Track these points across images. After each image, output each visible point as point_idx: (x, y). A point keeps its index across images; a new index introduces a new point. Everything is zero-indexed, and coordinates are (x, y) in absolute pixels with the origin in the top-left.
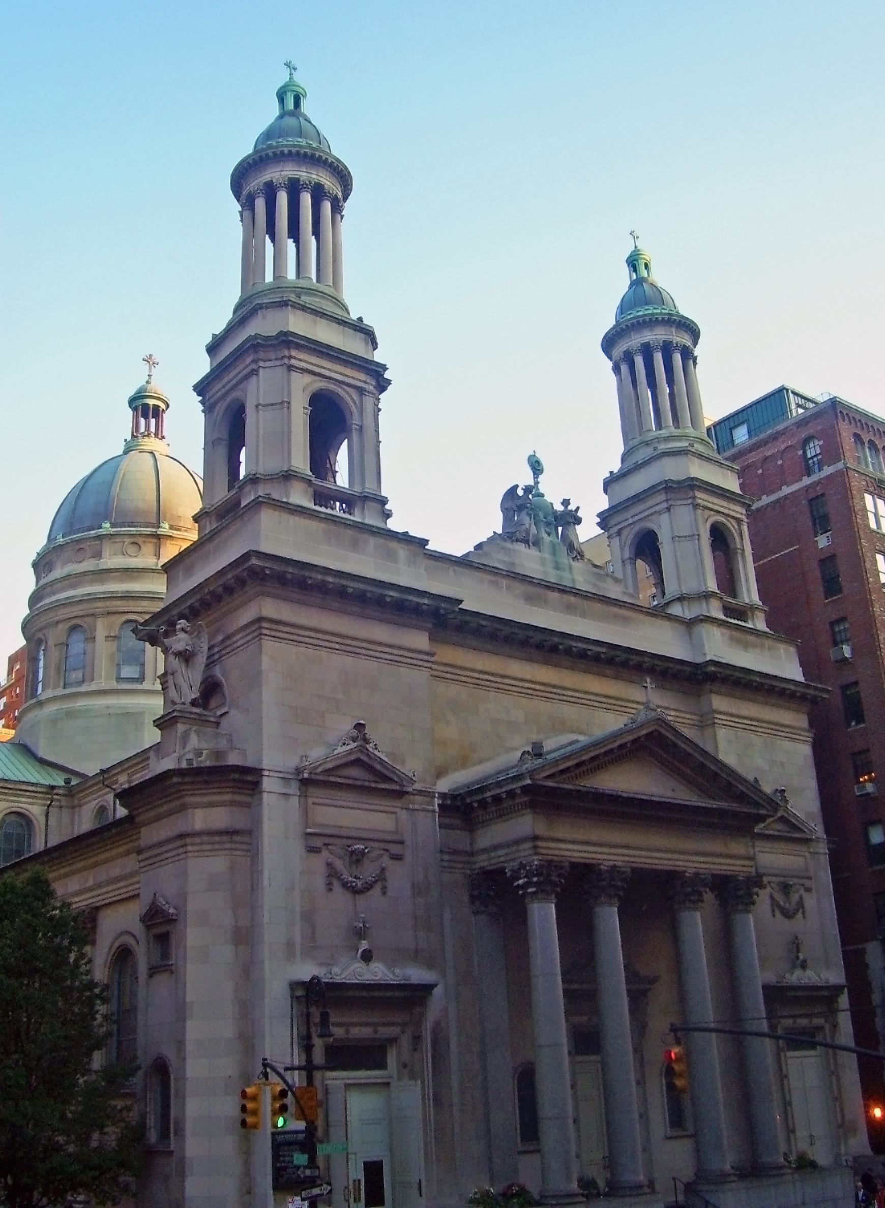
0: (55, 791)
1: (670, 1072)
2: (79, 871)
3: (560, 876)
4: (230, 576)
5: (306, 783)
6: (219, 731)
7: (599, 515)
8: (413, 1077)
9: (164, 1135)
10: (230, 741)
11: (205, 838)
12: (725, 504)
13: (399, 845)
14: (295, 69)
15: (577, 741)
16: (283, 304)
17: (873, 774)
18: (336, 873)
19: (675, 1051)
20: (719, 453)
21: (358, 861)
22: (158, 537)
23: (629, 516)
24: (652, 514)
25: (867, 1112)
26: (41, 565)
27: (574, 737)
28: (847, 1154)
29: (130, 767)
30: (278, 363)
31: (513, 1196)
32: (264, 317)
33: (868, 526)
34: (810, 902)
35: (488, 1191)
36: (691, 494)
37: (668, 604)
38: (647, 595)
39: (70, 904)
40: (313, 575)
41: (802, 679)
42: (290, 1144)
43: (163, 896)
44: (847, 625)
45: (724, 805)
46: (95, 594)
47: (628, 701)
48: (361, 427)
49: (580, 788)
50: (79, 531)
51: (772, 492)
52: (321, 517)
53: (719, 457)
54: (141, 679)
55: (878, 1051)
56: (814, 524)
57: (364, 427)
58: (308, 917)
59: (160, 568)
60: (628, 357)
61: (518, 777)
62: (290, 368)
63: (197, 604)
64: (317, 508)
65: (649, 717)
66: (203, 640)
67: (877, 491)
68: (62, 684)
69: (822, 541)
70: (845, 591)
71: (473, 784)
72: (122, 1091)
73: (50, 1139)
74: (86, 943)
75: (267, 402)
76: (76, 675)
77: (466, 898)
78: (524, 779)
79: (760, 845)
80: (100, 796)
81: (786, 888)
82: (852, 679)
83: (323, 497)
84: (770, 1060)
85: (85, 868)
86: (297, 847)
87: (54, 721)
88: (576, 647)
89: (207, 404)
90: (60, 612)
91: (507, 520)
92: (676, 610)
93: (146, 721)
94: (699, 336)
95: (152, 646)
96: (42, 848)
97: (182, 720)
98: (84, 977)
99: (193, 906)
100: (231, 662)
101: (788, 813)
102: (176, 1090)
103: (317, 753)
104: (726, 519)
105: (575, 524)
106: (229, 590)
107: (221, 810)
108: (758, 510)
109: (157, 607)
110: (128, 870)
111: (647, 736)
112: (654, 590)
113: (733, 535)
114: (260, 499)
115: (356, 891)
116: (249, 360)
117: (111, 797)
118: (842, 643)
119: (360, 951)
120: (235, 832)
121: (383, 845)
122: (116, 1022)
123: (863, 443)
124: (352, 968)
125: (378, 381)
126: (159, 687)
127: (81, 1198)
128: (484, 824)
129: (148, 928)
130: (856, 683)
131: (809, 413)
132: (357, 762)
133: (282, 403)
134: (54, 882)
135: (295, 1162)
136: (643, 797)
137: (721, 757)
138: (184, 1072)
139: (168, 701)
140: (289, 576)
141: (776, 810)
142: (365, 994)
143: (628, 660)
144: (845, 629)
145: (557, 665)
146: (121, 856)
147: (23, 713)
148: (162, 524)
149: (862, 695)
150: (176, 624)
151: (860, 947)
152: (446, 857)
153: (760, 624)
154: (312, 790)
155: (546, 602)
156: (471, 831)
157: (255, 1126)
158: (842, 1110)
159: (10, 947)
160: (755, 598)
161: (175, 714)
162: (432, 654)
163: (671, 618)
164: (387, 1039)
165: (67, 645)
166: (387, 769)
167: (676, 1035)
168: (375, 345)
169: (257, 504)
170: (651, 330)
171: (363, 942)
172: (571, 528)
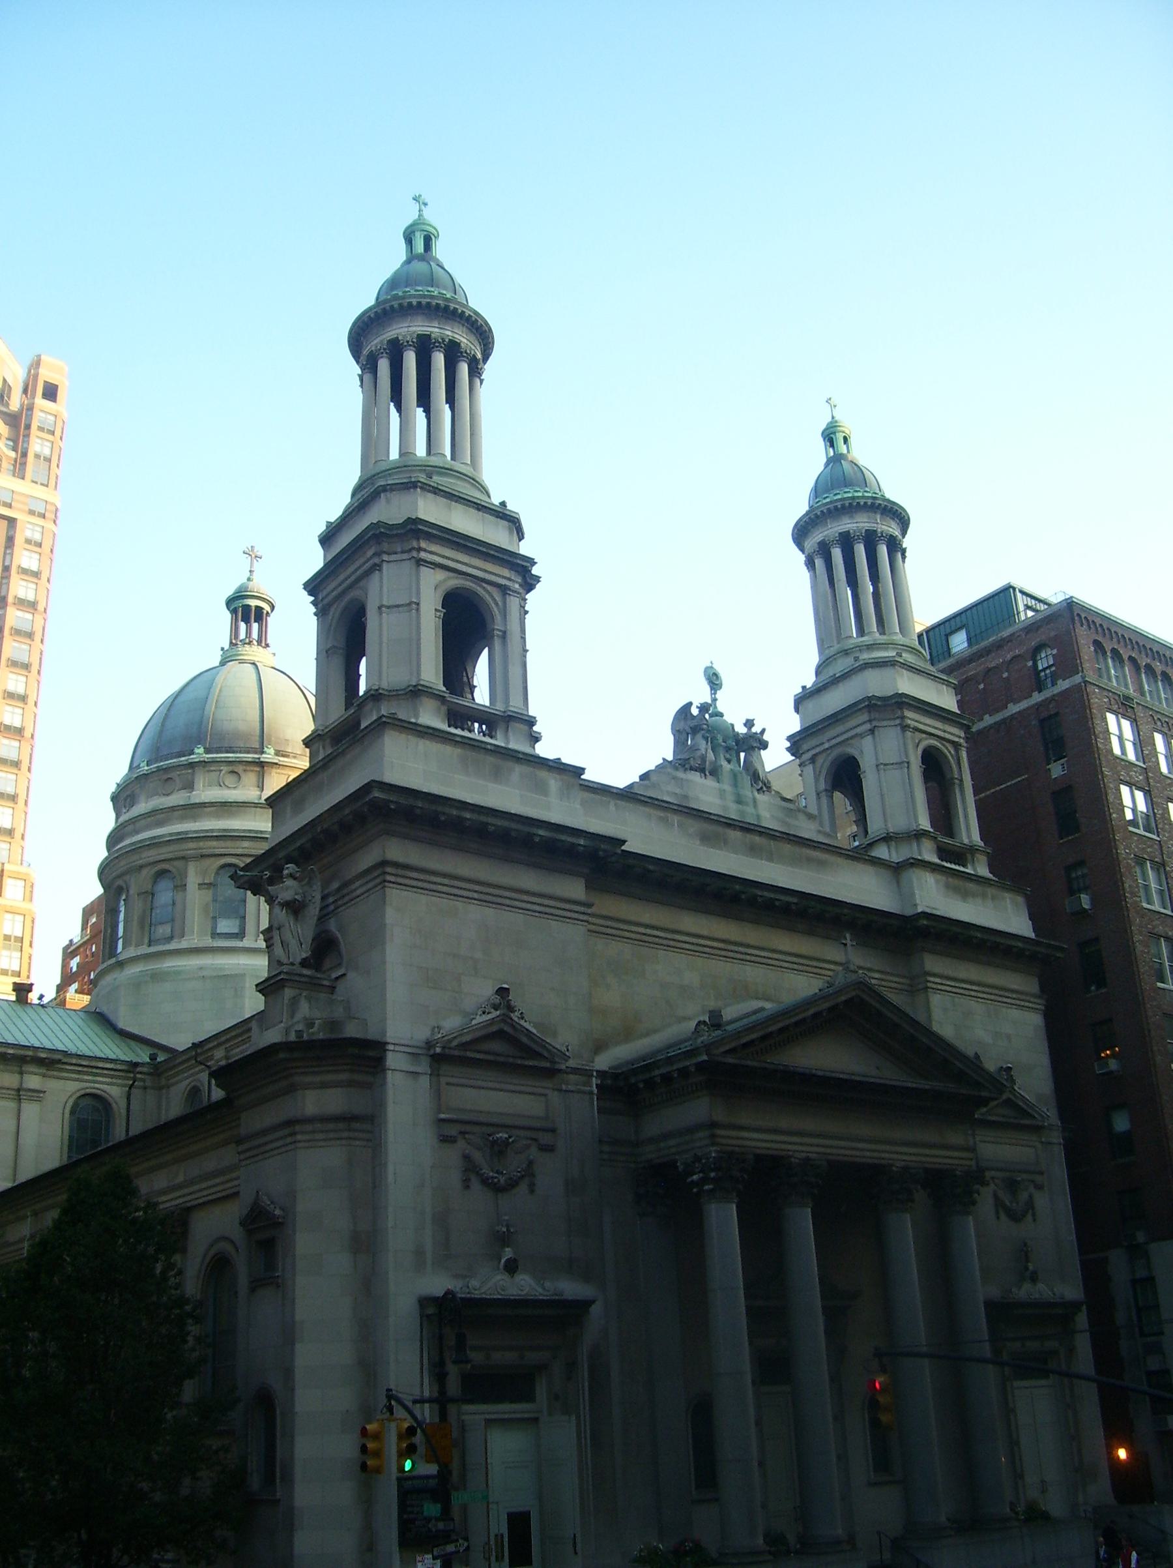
0: (139, 1069)
1: (873, 1405)
4: (347, 811)
7: (789, 738)
9: (269, 1478)
11: (318, 1126)
14: (425, 204)
15: (762, 1009)
16: (412, 486)
20: (932, 665)
22: (262, 765)
23: (825, 740)
24: (852, 738)
26: (122, 798)
29: (228, 1040)
30: (405, 556)
32: (388, 501)
34: (1041, 1201)
35: (656, 1548)
36: (899, 713)
37: (871, 845)
38: (846, 834)
39: (157, 1204)
40: (447, 810)
41: (1032, 935)
44: (1085, 871)
46: (187, 833)
48: (505, 632)
49: (767, 1066)
51: (997, 711)
53: (932, 669)
54: (241, 935)
57: (508, 633)
58: (442, 1220)
59: (264, 802)
60: (824, 550)
62: (419, 562)
64: (453, 730)
66: (315, 887)
68: (146, 941)
69: (1057, 770)
75: (391, 603)
76: (163, 930)
80: (192, 1075)
81: (1012, 1186)
86: (425, 1137)
87: (137, 985)
89: (320, 606)
91: (679, 743)
93: (247, 985)
95: (255, 895)
96: (123, 1137)
98: (173, 1292)
101: (1015, 1095)
103: (451, 1023)
105: (760, 749)
108: (980, 732)
109: (261, 848)
112: (854, 828)
113: (949, 762)
114: (384, 719)
115: (498, 1189)
116: (370, 553)
117: (204, 1076)
118: (1080, 891)
119: (503, 1261)
121: (529, 1134)
123: (1104, 653)
125: (524, 578)
126: (263, 945)
127: (169, 1556)
130: (1097, 939)
131: (1040, 616)
132: (500, 1035)
135: (425, 1514)
137: (935, 1028)
139: (274, 962)
140: (418, 811)
144: (1083, 876)
147: (100, 976)
148: (266, 749)
152: (606, 1148)
155: (726, 842)
157: (378, 1470)
161: (282, 976)
162: (590, 905)
163: (877, 862)
165: (153, 894)
166: (533, 1040)
169: (381, 725)
170: (851, 517)
171: (507, 1249)
172: (755, 754)
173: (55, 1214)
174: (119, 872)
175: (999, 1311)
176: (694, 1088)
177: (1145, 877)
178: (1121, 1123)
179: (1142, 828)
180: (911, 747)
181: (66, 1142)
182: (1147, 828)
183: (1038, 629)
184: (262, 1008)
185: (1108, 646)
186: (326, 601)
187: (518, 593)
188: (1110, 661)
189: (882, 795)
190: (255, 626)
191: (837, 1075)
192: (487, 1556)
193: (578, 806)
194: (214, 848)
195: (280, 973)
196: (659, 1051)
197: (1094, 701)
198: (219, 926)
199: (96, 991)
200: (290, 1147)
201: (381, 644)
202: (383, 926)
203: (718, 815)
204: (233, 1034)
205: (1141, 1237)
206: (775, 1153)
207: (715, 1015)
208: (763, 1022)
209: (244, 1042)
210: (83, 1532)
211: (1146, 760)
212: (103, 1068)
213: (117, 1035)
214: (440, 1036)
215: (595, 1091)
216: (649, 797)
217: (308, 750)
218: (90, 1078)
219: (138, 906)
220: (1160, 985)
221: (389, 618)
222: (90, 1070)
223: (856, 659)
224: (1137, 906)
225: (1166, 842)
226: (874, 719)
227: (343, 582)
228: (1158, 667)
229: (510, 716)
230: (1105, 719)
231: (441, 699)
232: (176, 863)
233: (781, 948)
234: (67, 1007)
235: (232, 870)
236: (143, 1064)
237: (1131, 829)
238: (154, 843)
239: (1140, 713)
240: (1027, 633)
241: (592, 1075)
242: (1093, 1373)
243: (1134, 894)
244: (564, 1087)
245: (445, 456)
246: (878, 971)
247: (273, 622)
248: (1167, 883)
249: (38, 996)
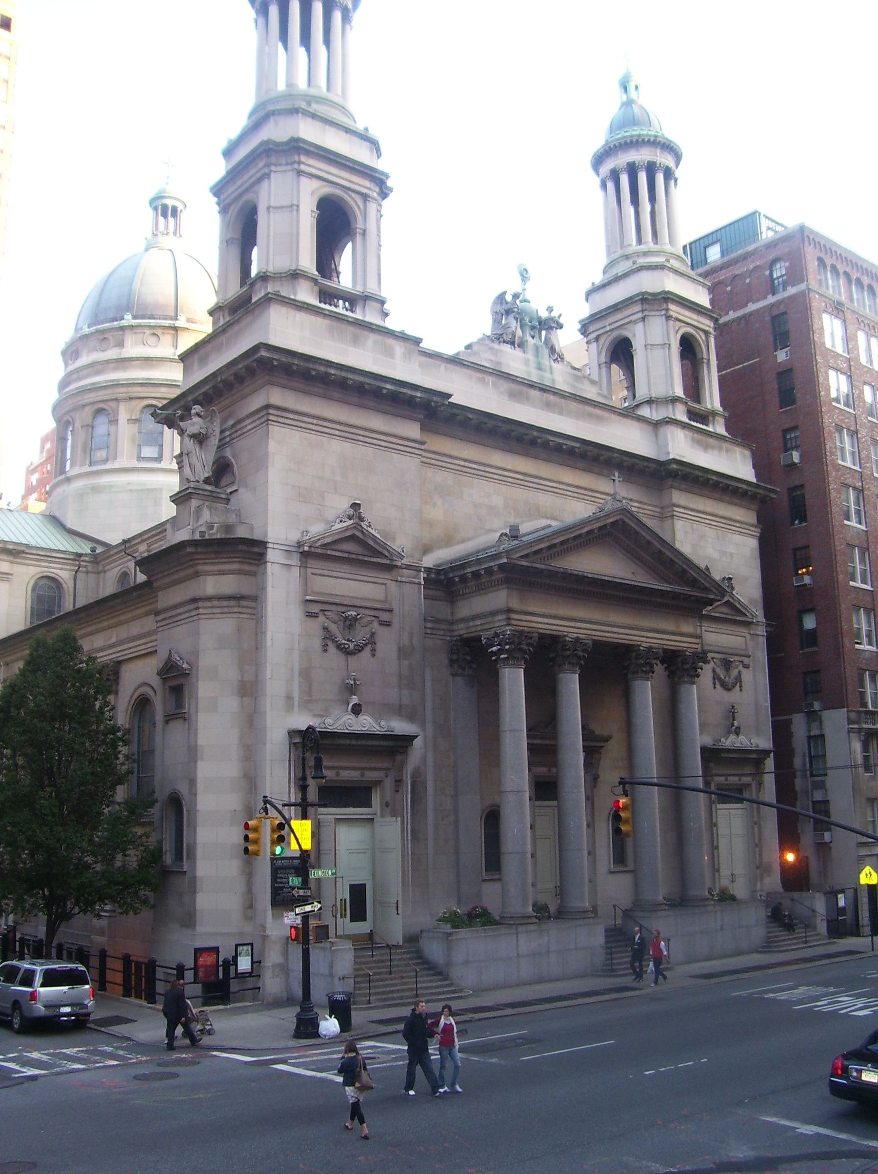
0: (83, 558)
2: (104, 629)
3: (528, 645)
4: (240, 366)
6: (229, 507)
7: (580, 322)
8: (394, 814)
9: (179, 855)
11: (216, 603)
12: (695, 316)
15: (550, 526)
16: (294, 111)
17: (811, 568)
19: (623, 801)
20: (693, 269)
22: (176, 329)
23: (607, 324)
25: (782, 856)
26: (71, 352)
28: (761, 890)
29: (149, 538)
30: (289, 167)
31: (477, 916)
32: (276, 123)
33: (823, 344)
34: (747, 676)
35: (455, 912)
36: (665, 306)
37: (637, 406)
38: (619, 396)
39: (95, 658)
40: (317, 367)
41: (754, 480)
43: (178, 653)
45: (677, 588)
46: (118, 380)
47: (597, 492)
48: (365, 231)
49: (549, 568)
51: (740, 308)
52: (325, 314)
53: (692, 274)
54: (159, 459)
56: (775, 340)
57: (367, 232)
58: (306, 674)
61: (493, 557)
62: (300, 173)
63: (211, 391)
64: (323, 306)
65: (615, 507)
66: (215, 424)
68: (88, 462)
69: (782, 356)
70: (799, 403)
71: (455, 560)
75: (278, 204)
76: (101, 454)
77: (446, 662)
78: (501, 558)
79: (707, 626)
80: (123, 563)
81: (727, 665)
83: (328, 295)
84: (703, 813)
85: (111, 627)
86: (296, 613)
87: (81, 495)
90: (86, 396)
91: (497, 322)
92: (645, 412)
93: (164, 497)
94: (681, 158)
95: (170, 428)
96: (71, 608)
97: (196, 496)
98: (108, 722)
99: (206, 661)
100: (241, 444)
101: (733, 598)
103: (316, 529)
104: (697, 332)
105: (557, 329)
106: (240, 379)
107: (231, 577)
108: (726, 324)
109: (174, 393)
111: (613, 524)
112: (625, 393)
113: (700, 345)
114: (270, 296)
115: (348, 653)
116: (261, 164)
117: (132, 565)
118: (792, 449)
119: (351, 705)
120: (242, 598)
121: (373, 613)
123: (825, 267)
125: (381, 189)
126: (176, 467)
127: (108, 907)
129: (164, 680)
130: (802, 486)
131: (777, 236)
132: (352, 538)
133: (291, 206)
136: (606, 578)
137: (678, 545)
138: (195, 805)
139: (184, 479)
140: (295, 368)
141: (723, 596)
144: (796, 438)
145: (535, 457)
146: (140, 617)
147: (53, 488)
148: (179, 317)
149: (807, 497)
152: (429, 625)
153: (720, 428)
154: (311, 562)
155: (528, 398)
156: (452, 603)
157: (256, 853)
159: (43, 695)
160: (717, 405)
161: (190, 491)
162: (423, 443)
163: (641, 419)
164: (372, 781)
165: (93, 427)
167: (624, 787)
169: (268, 300)
170: (637, 150)
171: (353, 697)
172: (553, 333)
173: (21, 664)
174: (67, 409)
175: (711, 755)
176: (496, 583)
178: (809, 622)
180: (672, 332)
181: (29, 609)
182: (847, 404)
183: (775, 246)
184: (175, 514)
185: (829, 262)
188: (829, 273)
189: (648, 368)
190: (171, 220)
191: (603, 578)
192: (334, 914)
195: (187, 489)
196: (471, 554)
201: (268, 237)
202: (267, 454)
204: (153, 533)
207: (514, 529)
208: (550, 536)
210: (46, 890)
213: (67, 534)
214: (307, 538)
215: (423, 582)
216: (472, 363)
218: (46, 564)
219: (82, 435)
220: (852, 583)
222: (46, 558)
223: (634, 263)
224: (834, 462)
225: (860, 415)
226: (646, 310)
227: (239, 188)
228: (866, 280)
230: (820, 319)
231: (315, 281)
232: (110, 403)
233: (566, 480)
235: (152, 410)
236: (86, 555)
237: (834, 404)
238: (94, 388)
239: (849, 315)
240: (767, 249)
241: (421, 571)
242: (775, 802)
243: (832, 454)
246: (638, 502)
248: (858, 447)
249: (7, 503)
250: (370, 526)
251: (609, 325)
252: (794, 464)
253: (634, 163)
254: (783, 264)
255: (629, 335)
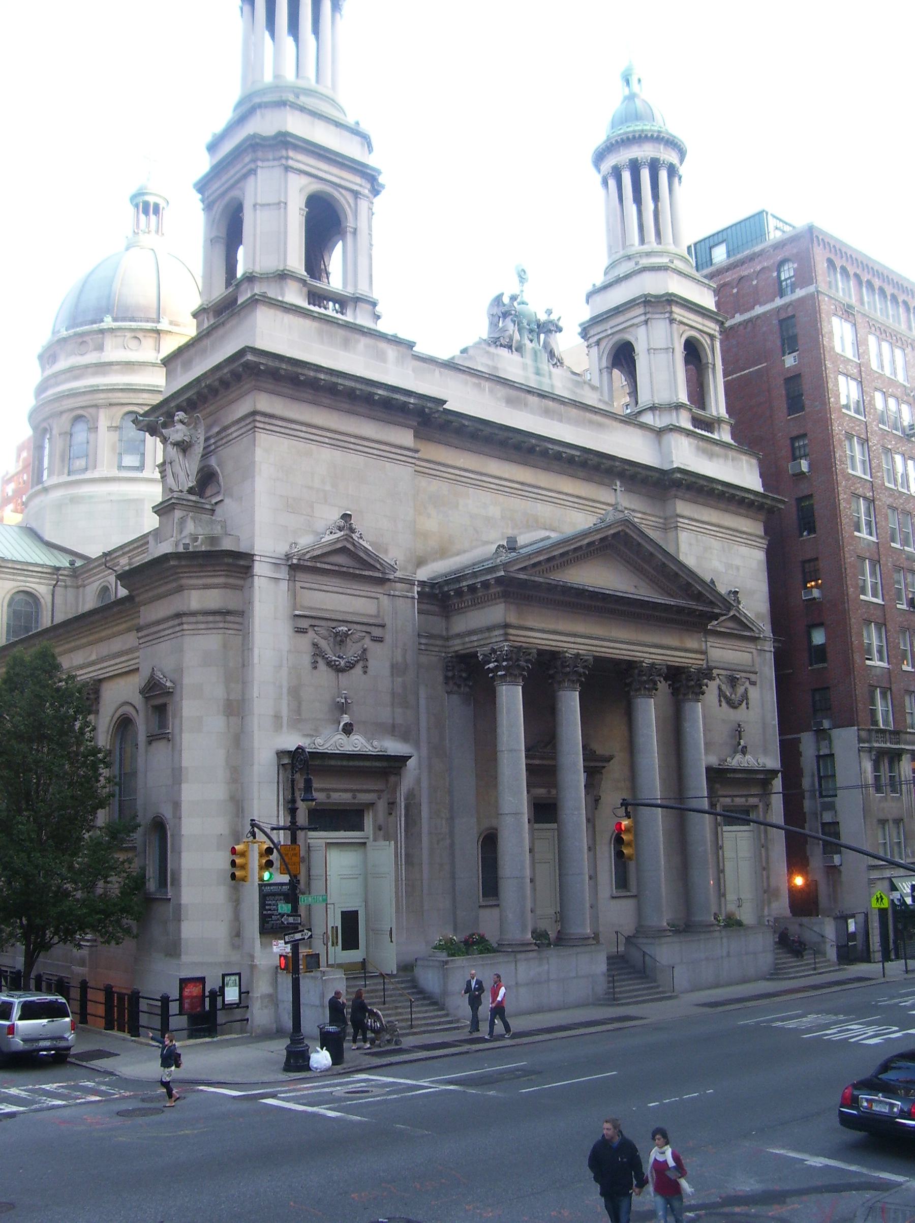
0: (60, 572)
1: (619, 841)
3: (527, 661)
4: (225, 371)
5: (294, 568)
6: (214, 518)
7: (580, 325)
8: (387, 838)
9: (163, 882)
10: (224, 527)
11: (200, 618)
12: (699, 319)
13: (380, 628)
15: (548, 538)
16: (282, 104)
17: (820, 581)
18: (321, 652)
19: (625, 823)
20: (697, 270)
21: (342, 641)
22: (158, 332)
23: (609, 327)
25: (790, 881)
26: (48, 356)
27: (547, 533)
28: (769, 915)
30: (276, 163)
31: (474, 943)
34: (754, 694)
35: (452, 939)
36: (668, 309)
37: (640, 413)
38: (621, 403)
39: (76, 676)
40: (306, 372)
41: (761, 490)
42: (273, 894)
44: (806, 442)
45: (681, 602)
48: (355, 229)
49: (550, 581)
50: (82, 325)
53: (697, 275)
54: (141, 468)
55: (804, 829)
56: (783, 345)
57: (358, 229)
58: (295, 692)
59: (160, 362)
60: (617, 173)
62: (287, 169)
63: (195, 397)
67: (844, 316)
68: (66, 471)
69: (790, 361)
71: (450, 574)
72: (124, 845)
73: (59, 887)
74: (90, 713)
75: (264, 202)
76: (80, 463)
77: (441, 679)
79: (712, 641)
81: (733, 681)
82: (806, 492)
83: (317, 297)
86: (284, 629)
88: (552, 449)
89: (206, 202)
91: (494, 325)
92: (648, 418)
95: (152, 436)
96: (49, 624)
98: (88, 743)
99: (189, 680)
101: (739, 613)
102: (173, 844)
103: (305, 541)
105: (556, 332)
106: (225, 384)
108: (732, 328)
109: (156, 399)
110: (128, 646)
111: (614, 535)
112: (627, 399)
113: (705, 349)
114: (256, 297)
115: (339, 670)
116: (247, 159)
117: (112, 578)
120: (229, 613)
121: (364, 628)
122: (119, 784)
123: (835, 269)
124: (334, 739)
125: (373, 186)
128: (460, 611)
129: (147, 699)
130: (810, 496)
131: (786, 236)
132: (343, 550)
133: (279, 203)
134: (59, 656)
135: (280, 911)
137: (682, 558)
139: (167, 490)
140: (283, 372)
141: (729, 610)
142: (345, 763)
143: (599, 464)
144: (804, 446)
147: (30, 498)
150: (174, 415)
151: (798, 736)
152: (423, 641)
153: (725, 435)
154: (300, 576)
155: (526, 405)
157: (244, 879)
158: (768, 878)
159: (20, 715)
160: (723, 412)
161: (173, 501)
162: (417, 451)
163: (643, 426)
165: (71, 435)
167: (626, 809)
168: (370, 148)
169: (254, 301)
170: (640, 146)
175: (717, 775)
177: (869, 637)
178: (819, 638)
179: (852, 410)
180: (676, 336)
182: (857, 411)
185: (838, 263)
186: (211, 198)
187: (368, 197)
189: (651, 374)
190: (153, 218)
193: (411, 372)
194: (119, 398)
197: (824, 307)
198: (123, 460)
199: (26, 511)
200: (179, 634)
202: (253, 463)
203: (520, 384)
204: (135, 545)
205: (826, 724)
206: (553, 649)
207: (512, 540)
209: (143, 552)
211: (861, 357)
212: (32, 571)
214: (296, 550)
215: (417, 597)
217: (195, 320)
219: (59, 443)
220: (862, 597)
221: (263, 216)
223: (637, 264)
224: (843, 471)
225: (870, 423)
227: (226, 182)
229: (358, 298)
231: (304, 282)
233: (566, 490)
234: (5, 522)
235: (133, 417)
236: (65, 568)
237: (844, 411)
239: (859, 319)
244: (392, 592)
245: (308, 79)
246: (640, 512)
247: (167, 214)
248: (869, 455)
250: (361, 538)
251: (611, 328)
252: (803, 473)
253: (637, 160)
254: (791, 265)
255: (631, 339)
